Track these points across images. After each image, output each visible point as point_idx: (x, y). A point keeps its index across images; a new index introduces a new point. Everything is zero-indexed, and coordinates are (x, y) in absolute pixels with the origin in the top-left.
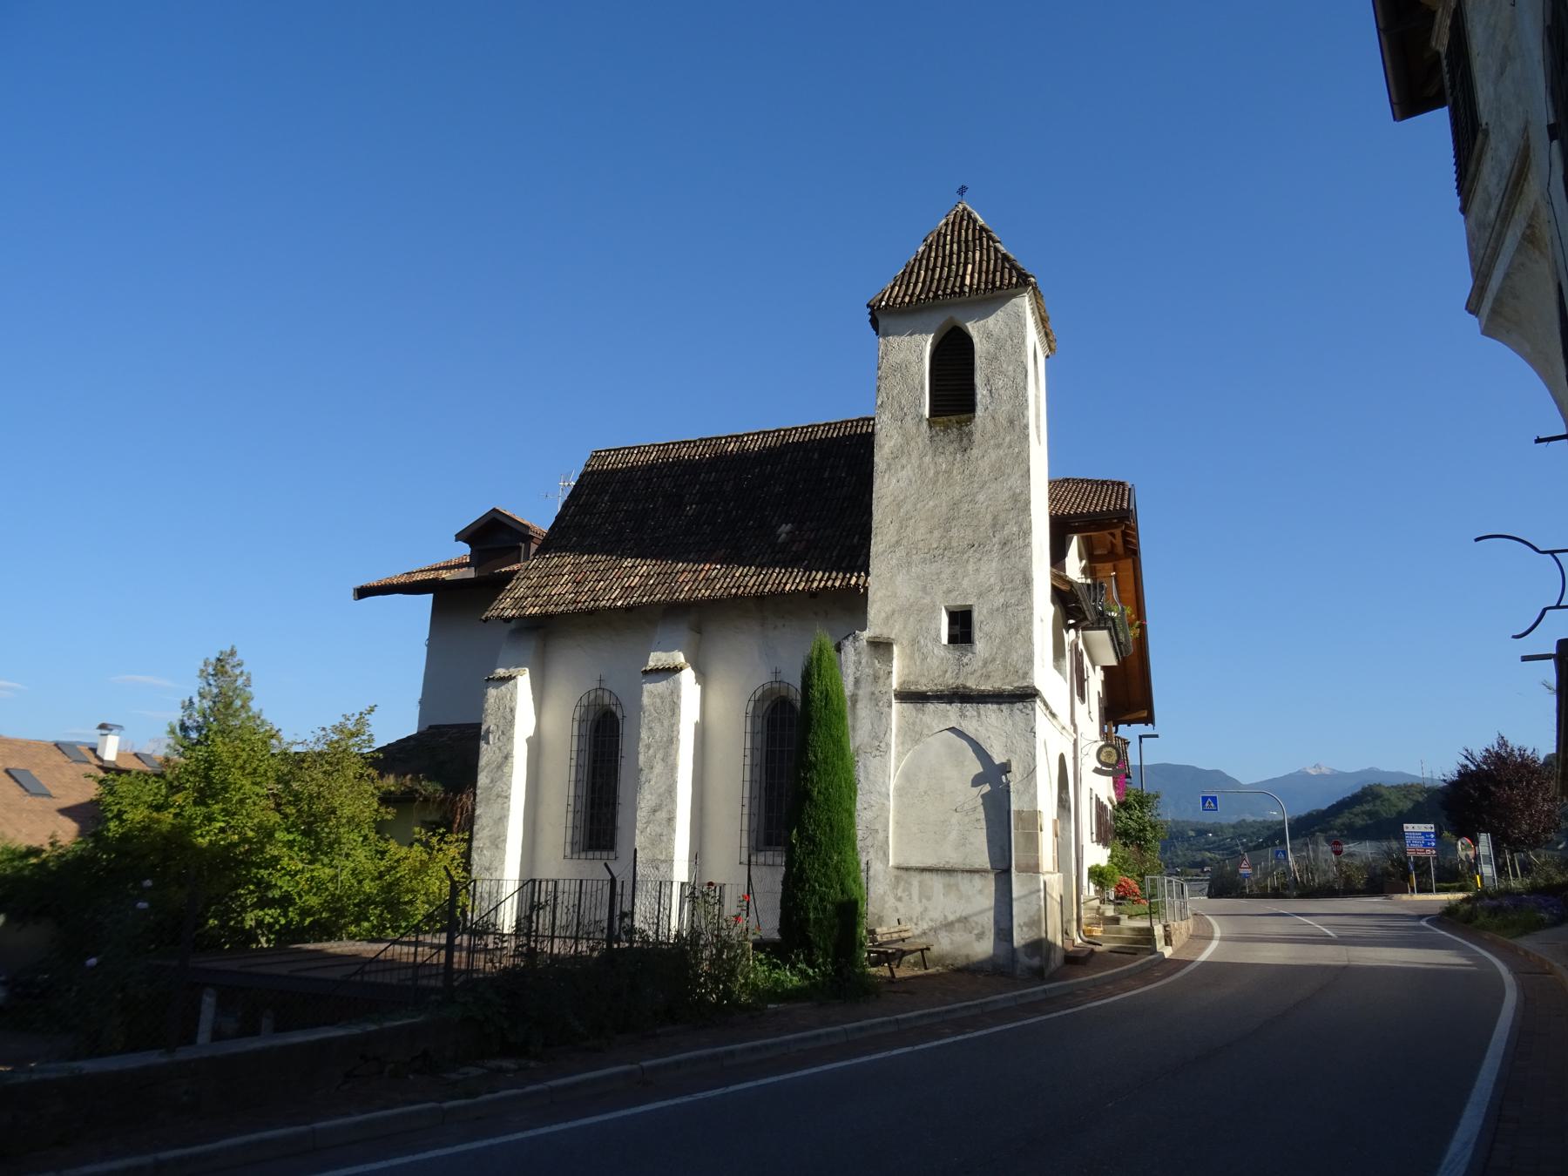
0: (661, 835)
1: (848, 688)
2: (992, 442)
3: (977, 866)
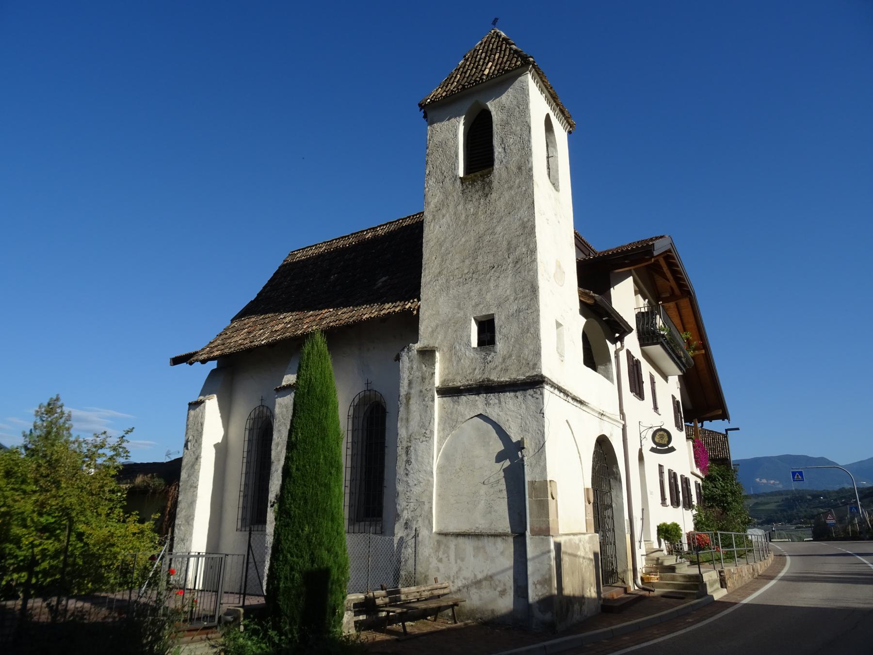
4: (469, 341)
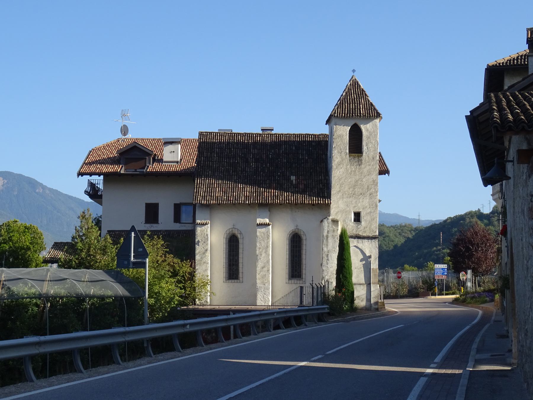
0: (265, 275)
1: (325, 234)
2: (368, 164)
3: (361, 283)
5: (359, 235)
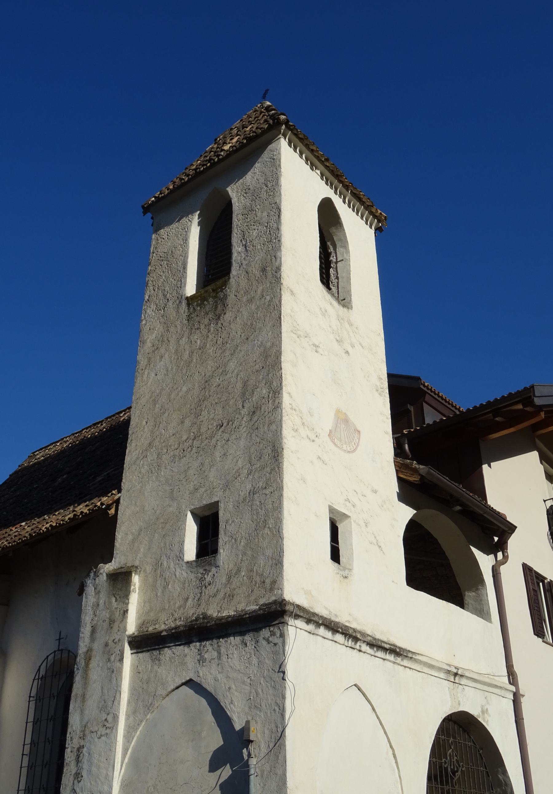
4: (181, 551)
5: (205, 616)
